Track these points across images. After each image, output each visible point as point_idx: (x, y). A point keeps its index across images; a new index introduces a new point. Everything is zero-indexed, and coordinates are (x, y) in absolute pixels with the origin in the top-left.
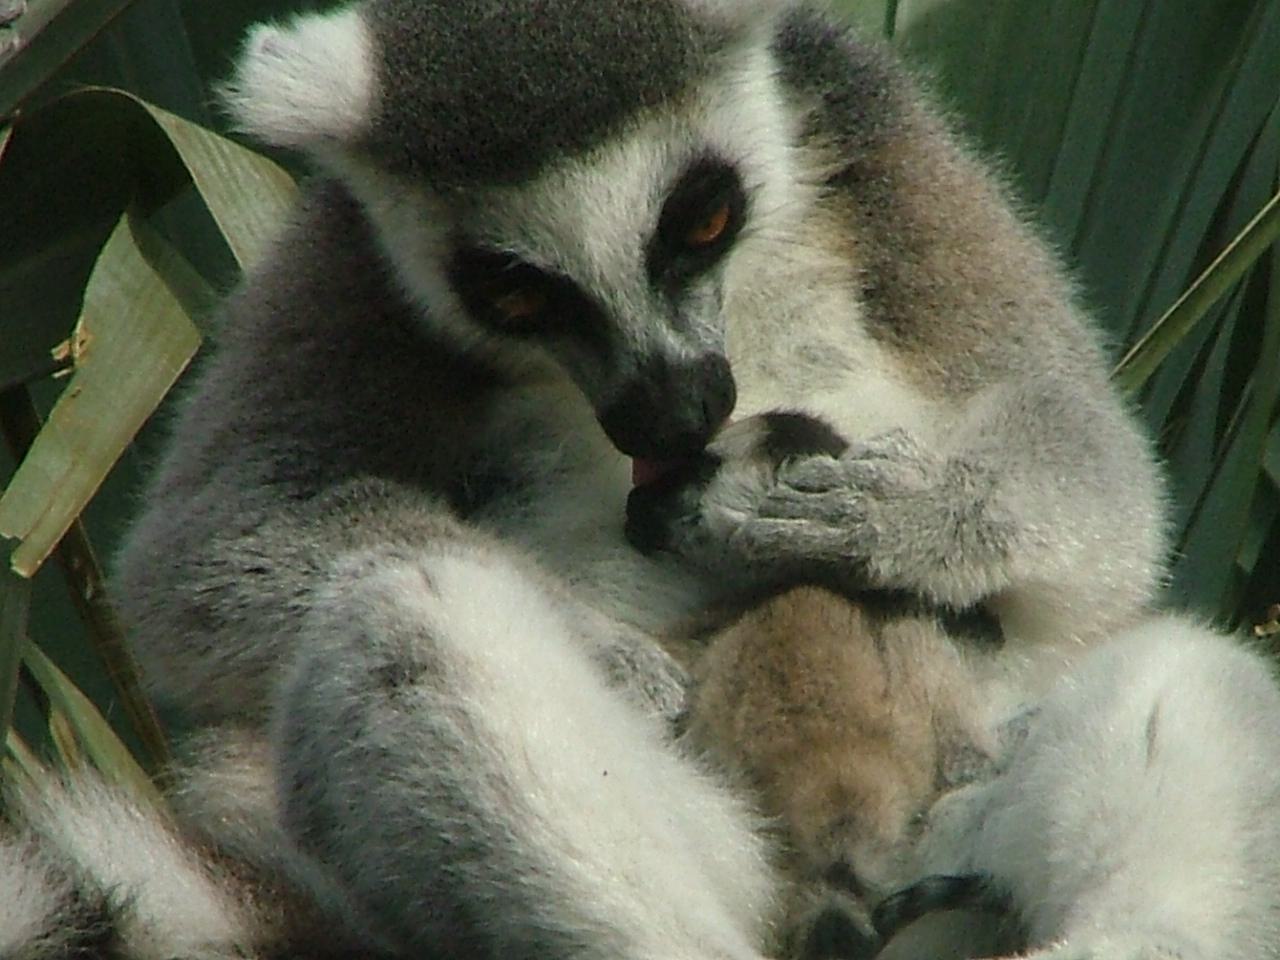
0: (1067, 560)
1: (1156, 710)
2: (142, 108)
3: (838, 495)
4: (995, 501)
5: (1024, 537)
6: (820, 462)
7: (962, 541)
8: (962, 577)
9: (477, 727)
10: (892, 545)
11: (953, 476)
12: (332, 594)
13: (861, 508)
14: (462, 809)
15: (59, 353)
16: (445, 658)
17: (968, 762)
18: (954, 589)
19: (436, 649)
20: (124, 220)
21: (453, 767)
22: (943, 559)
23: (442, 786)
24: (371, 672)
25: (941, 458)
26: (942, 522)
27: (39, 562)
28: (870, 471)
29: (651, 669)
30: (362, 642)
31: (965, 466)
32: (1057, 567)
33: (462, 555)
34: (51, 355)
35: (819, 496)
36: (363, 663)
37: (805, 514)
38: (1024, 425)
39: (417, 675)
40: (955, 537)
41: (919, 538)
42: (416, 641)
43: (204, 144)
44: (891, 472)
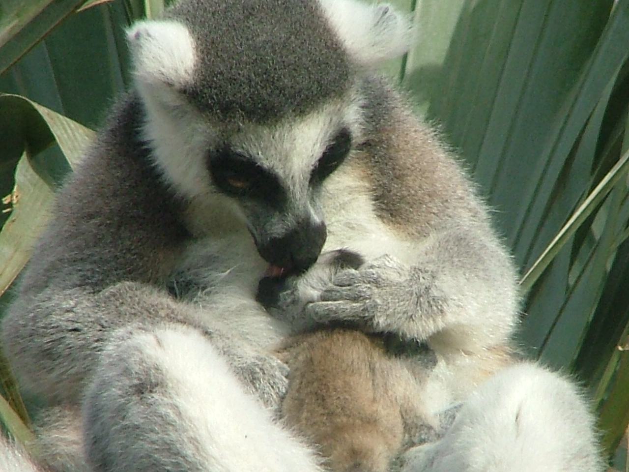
0: (472, 313)
1: (520, 409)
2: (31, 105)
3: (357, 287)
4: (435, 286)
5: (450, 302)
6: (348, 272)
7: (420, 306)
8: (422, 326)
9: (183, 414)
10: (385, 309)
11: (414, 274)
12: (111, 348)
13: (369, 293)
14: (175, 454)
15: (6, 200)
16: (168, 379)
17: (422, 432)
18: (418, 331)
19: (163, 375)
20: (25, 153)
21: (171, 433)
22: (411, 317)
23: (166, 443)
24: (130, 387)
25: (407, 267)
26: (410, 297)
27: (3, 292)
28: (373, 274)
29: (272, 373)
30: (127, 372)
31: (420, 270)
32: (468, 317)
33: (175, 329)
34: (2, 201)
35: (348, 288)
36: (127, 382)
37: (341, 298)
38: (447, 249)
39: (153, 388)
40: (417, 305)
41: (399, 306)
42: (153, 371)
43: (62, 124)
44: (383, 274)
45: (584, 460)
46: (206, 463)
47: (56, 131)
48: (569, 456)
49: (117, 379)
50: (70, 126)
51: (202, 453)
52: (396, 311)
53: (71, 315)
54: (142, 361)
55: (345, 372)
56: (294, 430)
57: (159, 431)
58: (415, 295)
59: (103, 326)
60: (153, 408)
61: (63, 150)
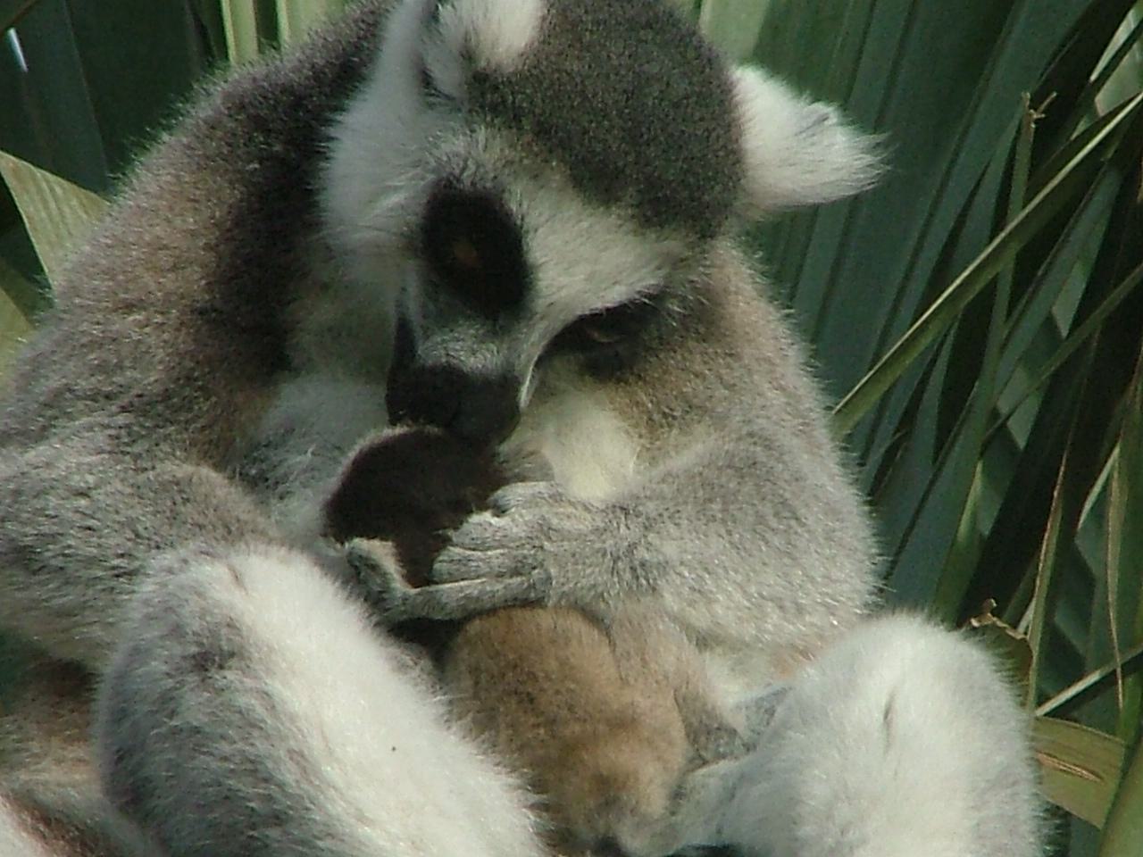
12: (150, 588)
17: (722, 741)
21: (257, 743)
24: (184, 658)
30: (177, 631)
36: (178, 650)
43: (40, 191)
45: (1009, 791)
46: (322, 797)
47: (26, 205)
48: (983, 785)
49: (161, 643)
50: (52, 190)
51: (312, 778)
52: (579, 585)
53: (83, 502)
54: (204, 613)
55: (553, 642)
56: (483, 742)
57: (236, 738)
58: (609, 556)
59: (138, 535)
60: (226, 695)
61: (37, 248)
